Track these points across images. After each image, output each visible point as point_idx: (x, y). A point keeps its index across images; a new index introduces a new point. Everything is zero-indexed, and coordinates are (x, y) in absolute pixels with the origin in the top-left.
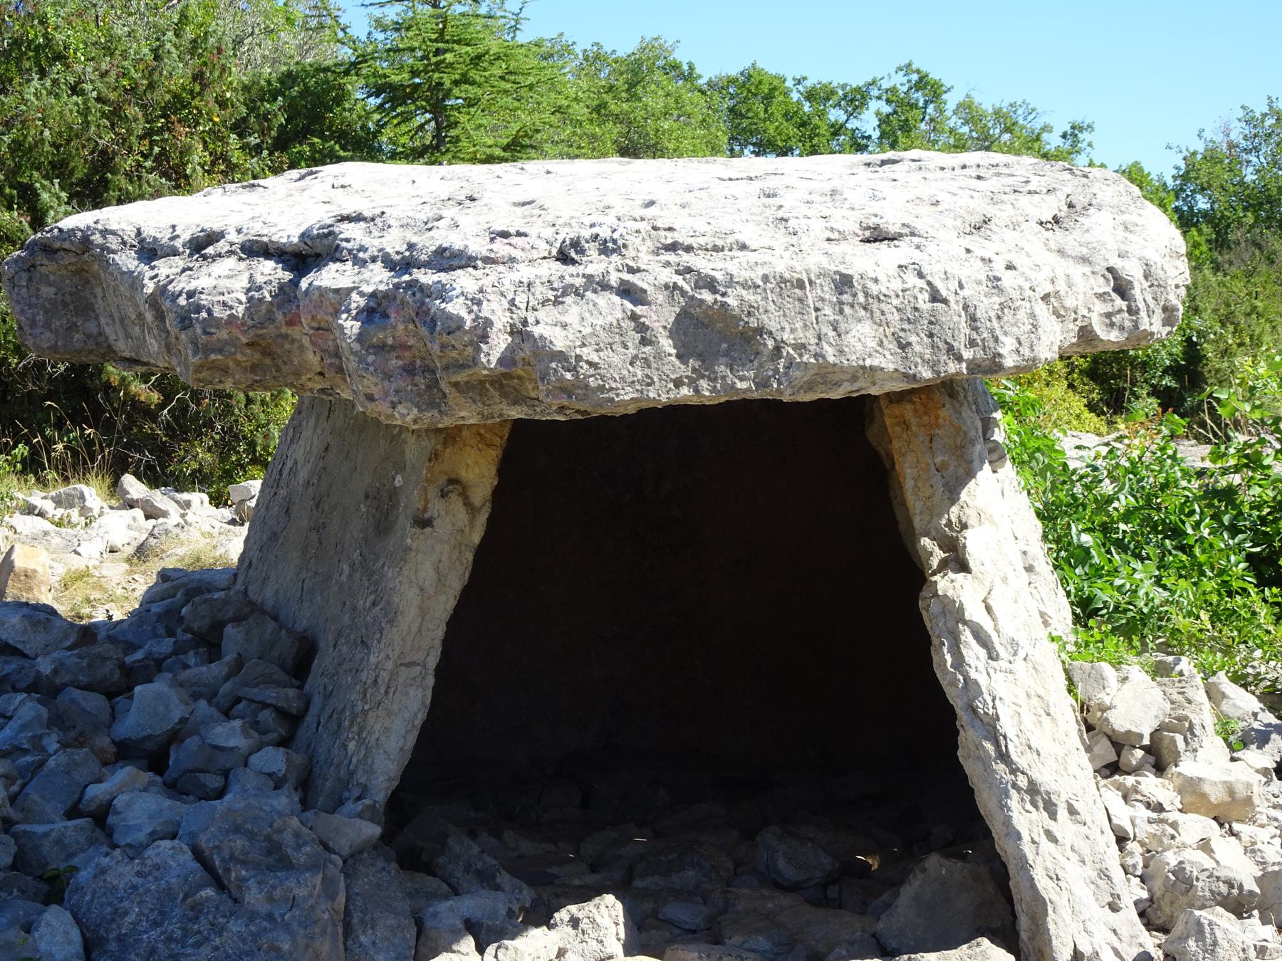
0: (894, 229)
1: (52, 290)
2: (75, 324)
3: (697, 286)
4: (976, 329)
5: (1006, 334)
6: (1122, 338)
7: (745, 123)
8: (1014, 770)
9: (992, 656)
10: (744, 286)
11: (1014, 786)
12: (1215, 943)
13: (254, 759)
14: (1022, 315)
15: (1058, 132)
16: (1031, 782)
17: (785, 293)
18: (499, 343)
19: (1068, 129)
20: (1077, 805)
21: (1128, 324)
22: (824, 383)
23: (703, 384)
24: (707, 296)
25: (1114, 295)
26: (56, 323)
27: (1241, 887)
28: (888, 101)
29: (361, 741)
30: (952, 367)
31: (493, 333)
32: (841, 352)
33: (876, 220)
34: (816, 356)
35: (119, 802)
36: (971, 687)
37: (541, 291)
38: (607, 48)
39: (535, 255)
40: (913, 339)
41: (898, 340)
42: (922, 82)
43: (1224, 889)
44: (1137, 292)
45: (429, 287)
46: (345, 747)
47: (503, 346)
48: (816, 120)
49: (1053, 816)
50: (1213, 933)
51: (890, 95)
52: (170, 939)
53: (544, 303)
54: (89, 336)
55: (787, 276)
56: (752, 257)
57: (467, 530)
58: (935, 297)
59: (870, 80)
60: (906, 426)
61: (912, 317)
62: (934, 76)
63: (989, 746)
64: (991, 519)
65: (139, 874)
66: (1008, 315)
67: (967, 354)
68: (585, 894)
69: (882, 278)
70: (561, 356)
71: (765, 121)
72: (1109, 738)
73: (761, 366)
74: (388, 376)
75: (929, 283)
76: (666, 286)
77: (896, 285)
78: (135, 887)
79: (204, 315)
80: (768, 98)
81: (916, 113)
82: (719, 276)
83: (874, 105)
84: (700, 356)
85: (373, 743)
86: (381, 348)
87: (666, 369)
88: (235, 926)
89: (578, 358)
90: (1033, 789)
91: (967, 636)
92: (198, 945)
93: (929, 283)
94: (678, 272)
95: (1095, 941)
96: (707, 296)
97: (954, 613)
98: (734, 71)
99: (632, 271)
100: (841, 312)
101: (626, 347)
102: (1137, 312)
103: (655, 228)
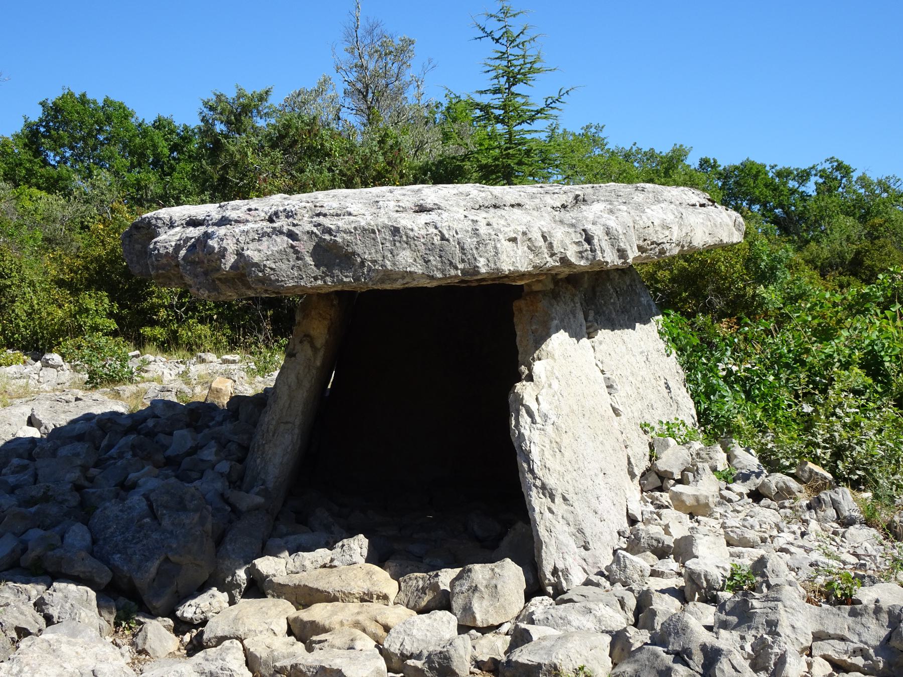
0: (429, 206)
3: (323, 232)
4: (465, 254)
5: (481, 256)
6: (588, 264)
7: (744, 189)
9: (534, 422)
10: (345, 232)
11: (534, 485)
12: (625, 567)
13: (218, 467)
14: (489, 247)
16: (543, 484)
17: (366, 236)
18: (231, 259)
20: (566, 495)
21: (590, 257)
22: (389, 279)
23: (328, 279)
24: (327, 237)
25: (584, 243)
27: (663, 543)
28: (821, 177)
30: (453, 272)
31: (227, 254)
32: (395, 264)
33: (421, 202)
34: (382, 266)
35: (141, 482)
36: (521, 436)
37: (253, 235)
38: (657, 151)
39: (258, 219)
40: (431, 258)
41: (424, 258)
42: (840, 167)
43: (655, 543)
44: (596, 241)
47: (233, 260)
48: (781, 188)
49: (553, 501)
50: (624, 562)
51: (822, 174)
52: (126, 540)
53: (253, 240)
55: (366, 227)
56: (352, 218)
57: (312, 359)
58: (443, 238)
59: (811, 166)
60: (520, 310)
61: (431, 248)
62: (846, 163)
63: (525, 465)
64: (553, 358)
65: (121, 511)
66: (482, 248)
67: (460, 266)
68: (351, 534)
69: (416, 229)
70: (256, 265)
71: (754, 188)
72: (657, 474)
73: (356, 270)
74: (196, 276)
75: (440, 231)
76: (308, 232)
77: (423, 232)
78: (117, 516)
80: (756, 177)
81: (836, 183)
82: (333, 227)
83: (813, 179)
84: (326, 266)
87: (309, 272)
88: (155, 536)
89: (265, 266)
90: (544, 487)
91: (523, 412)
92: (137, 543)
93: (440, 231)
94: (315, 226)
95: (567, 563)
96: (327, 237)
97: (520, 400)
98: (737, 163)
99: (294, 225)
100: (395, 245)
101: (289, 261)
102: (595, 251)
103: (315, 206)
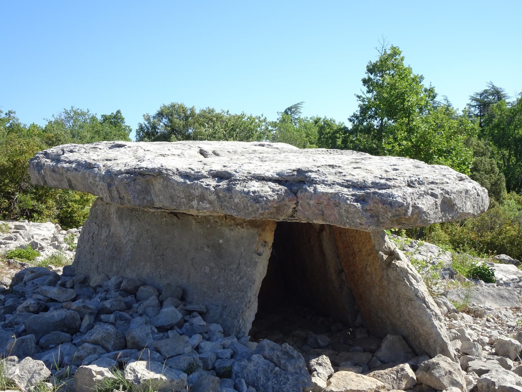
1: (140, 187)
2: (145, 197)
8: (432, 311)
15: (4, 113)
16: (436, 313)
19: (7, 112)
24: (447, 196)
26: (140, 197)
29: (243, 319)
45: (383, 194)
46: (239, 321)
54: (148, 201)
63: (424, 305)
70: (425, 213)
79: (265, 199)
85: (246, 320)
86: (366, 210)
96: (447, 196)
